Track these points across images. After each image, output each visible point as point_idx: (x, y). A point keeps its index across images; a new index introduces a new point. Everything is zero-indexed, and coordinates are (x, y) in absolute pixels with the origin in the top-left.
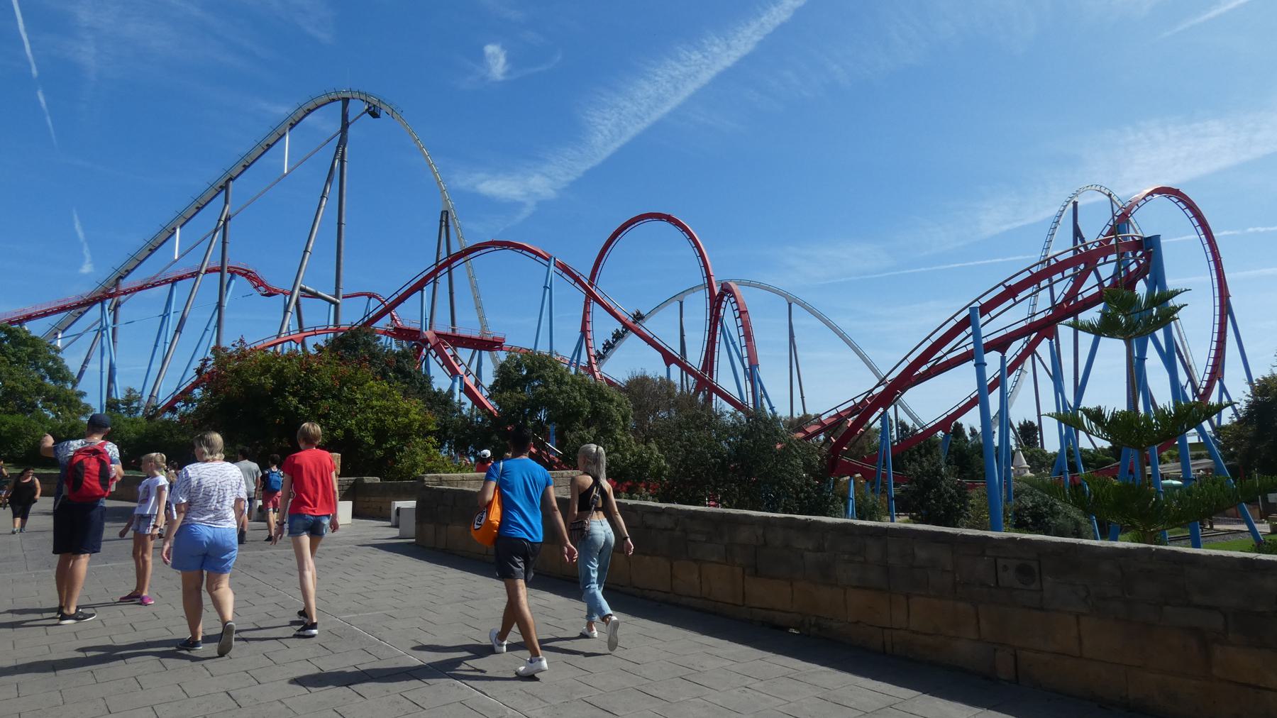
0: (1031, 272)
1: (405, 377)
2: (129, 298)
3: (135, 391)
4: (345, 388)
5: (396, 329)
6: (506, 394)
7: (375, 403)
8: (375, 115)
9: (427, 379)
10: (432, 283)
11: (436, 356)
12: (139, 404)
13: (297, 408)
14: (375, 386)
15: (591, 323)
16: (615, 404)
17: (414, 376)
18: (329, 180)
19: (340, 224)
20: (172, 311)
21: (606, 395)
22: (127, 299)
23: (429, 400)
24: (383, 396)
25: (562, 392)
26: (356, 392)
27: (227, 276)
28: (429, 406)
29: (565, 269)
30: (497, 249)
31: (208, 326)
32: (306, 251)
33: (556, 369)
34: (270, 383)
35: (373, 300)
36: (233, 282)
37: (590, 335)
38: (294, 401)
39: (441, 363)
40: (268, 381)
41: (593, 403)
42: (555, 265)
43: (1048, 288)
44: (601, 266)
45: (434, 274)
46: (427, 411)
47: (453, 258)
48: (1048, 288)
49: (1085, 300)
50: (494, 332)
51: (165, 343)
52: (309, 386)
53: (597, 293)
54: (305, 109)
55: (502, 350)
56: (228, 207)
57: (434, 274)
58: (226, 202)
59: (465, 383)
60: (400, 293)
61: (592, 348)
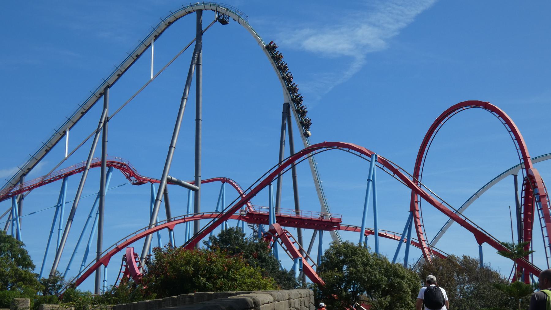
1: (262, 262)
3: (58, 272)
4: (230, 272)
5: (248, 214)
6: (328, 273)
7: (247, 280)
8: (224, 22)
9: (276, 263)
10: (277, 179)
11: (282, 243)
12: (61, 283)
13: (205, 284)
14: (247, 270)
15: (419, 203)
16: (406, 280)
17: (268, 261)
18: (188, 83)
19: (198, 120)
20: (64, 202)
21: (399, 273)
23: (278, 277)
24: (250, 276)
25: (366, 271)
26: (236, 274)
27: (106, 169)
28: (279, 281)
29: (385, 163)
30: (328, 149)
31: (91, 213)
32: (171, 147)
33: (363, 255)
34: (192, 270)
35: (226, 184)
36: (111, 174)
37: (418, 214)
38: (204, 280)
39: (286, 248)
40: (191, 269)
41: (389, 279)
42: (376, 161)
44: (426, 151)
45: (277, 173)
46: (277, 285)
47: (295, 157)
50: (334, 213)
51: (59, 229)
52: (211, 271)
53: (422, 189)
54: (167, 22)
55: (339, 229)
56: (106, 110)
57: (277, 173)
58: (105, 107)
59: (303, 264)
60: (252, 188)
61: (420, 226)
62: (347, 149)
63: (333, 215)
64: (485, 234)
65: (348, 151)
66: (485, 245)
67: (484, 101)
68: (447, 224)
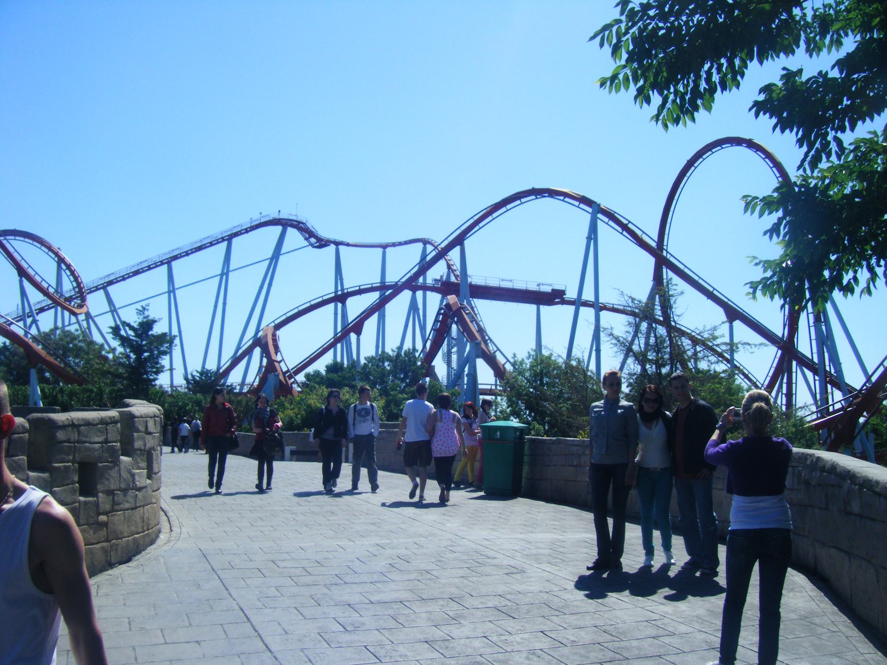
30: (538, 197)
62: (562, 198)
63: (555, 286)
64: (736, 309)
65: (563, 200)
66: (737, 324)
67: (747, 137)
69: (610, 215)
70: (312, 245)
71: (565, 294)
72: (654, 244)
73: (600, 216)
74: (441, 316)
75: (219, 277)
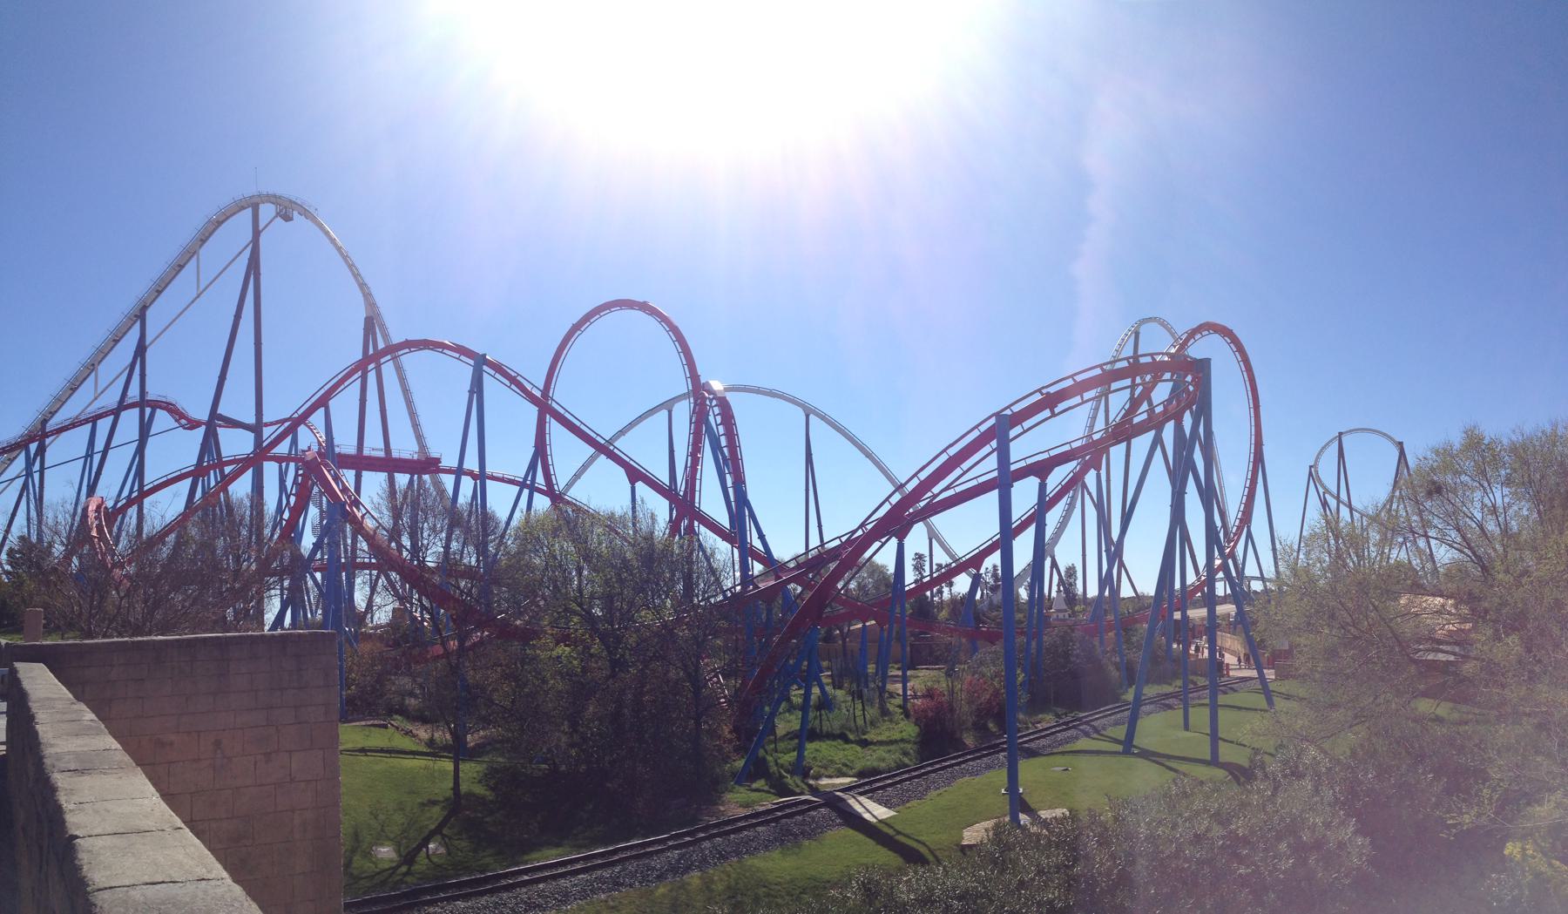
0: (1074, 380)
2: (55, 439)
8: (288, 218)
22: (52, 441)
43: (1129, 389)
48: (1129, 389)
49: (988, 442)
65: (441, 352)
66: (640, 485)
68: (592, 460)
69: (498, 368)
70: (182, 426)
71: (440, 462)
72: (538, 394)
73: (485, 368)
74: (300, 478)
75: (83, 459)
